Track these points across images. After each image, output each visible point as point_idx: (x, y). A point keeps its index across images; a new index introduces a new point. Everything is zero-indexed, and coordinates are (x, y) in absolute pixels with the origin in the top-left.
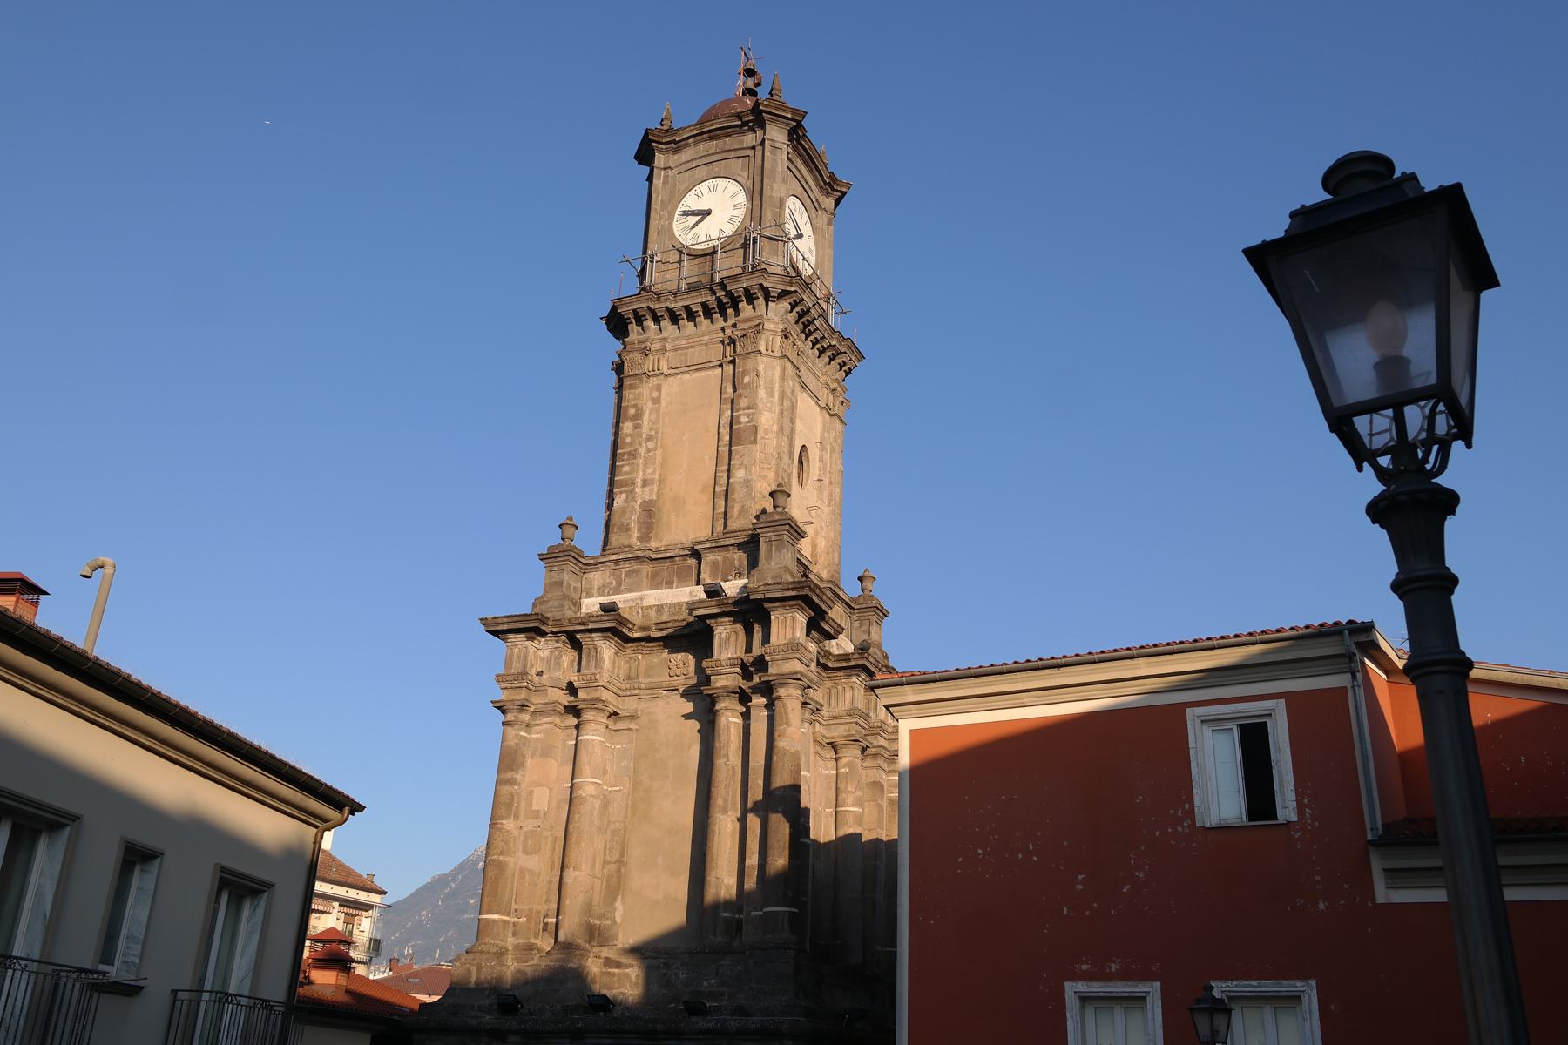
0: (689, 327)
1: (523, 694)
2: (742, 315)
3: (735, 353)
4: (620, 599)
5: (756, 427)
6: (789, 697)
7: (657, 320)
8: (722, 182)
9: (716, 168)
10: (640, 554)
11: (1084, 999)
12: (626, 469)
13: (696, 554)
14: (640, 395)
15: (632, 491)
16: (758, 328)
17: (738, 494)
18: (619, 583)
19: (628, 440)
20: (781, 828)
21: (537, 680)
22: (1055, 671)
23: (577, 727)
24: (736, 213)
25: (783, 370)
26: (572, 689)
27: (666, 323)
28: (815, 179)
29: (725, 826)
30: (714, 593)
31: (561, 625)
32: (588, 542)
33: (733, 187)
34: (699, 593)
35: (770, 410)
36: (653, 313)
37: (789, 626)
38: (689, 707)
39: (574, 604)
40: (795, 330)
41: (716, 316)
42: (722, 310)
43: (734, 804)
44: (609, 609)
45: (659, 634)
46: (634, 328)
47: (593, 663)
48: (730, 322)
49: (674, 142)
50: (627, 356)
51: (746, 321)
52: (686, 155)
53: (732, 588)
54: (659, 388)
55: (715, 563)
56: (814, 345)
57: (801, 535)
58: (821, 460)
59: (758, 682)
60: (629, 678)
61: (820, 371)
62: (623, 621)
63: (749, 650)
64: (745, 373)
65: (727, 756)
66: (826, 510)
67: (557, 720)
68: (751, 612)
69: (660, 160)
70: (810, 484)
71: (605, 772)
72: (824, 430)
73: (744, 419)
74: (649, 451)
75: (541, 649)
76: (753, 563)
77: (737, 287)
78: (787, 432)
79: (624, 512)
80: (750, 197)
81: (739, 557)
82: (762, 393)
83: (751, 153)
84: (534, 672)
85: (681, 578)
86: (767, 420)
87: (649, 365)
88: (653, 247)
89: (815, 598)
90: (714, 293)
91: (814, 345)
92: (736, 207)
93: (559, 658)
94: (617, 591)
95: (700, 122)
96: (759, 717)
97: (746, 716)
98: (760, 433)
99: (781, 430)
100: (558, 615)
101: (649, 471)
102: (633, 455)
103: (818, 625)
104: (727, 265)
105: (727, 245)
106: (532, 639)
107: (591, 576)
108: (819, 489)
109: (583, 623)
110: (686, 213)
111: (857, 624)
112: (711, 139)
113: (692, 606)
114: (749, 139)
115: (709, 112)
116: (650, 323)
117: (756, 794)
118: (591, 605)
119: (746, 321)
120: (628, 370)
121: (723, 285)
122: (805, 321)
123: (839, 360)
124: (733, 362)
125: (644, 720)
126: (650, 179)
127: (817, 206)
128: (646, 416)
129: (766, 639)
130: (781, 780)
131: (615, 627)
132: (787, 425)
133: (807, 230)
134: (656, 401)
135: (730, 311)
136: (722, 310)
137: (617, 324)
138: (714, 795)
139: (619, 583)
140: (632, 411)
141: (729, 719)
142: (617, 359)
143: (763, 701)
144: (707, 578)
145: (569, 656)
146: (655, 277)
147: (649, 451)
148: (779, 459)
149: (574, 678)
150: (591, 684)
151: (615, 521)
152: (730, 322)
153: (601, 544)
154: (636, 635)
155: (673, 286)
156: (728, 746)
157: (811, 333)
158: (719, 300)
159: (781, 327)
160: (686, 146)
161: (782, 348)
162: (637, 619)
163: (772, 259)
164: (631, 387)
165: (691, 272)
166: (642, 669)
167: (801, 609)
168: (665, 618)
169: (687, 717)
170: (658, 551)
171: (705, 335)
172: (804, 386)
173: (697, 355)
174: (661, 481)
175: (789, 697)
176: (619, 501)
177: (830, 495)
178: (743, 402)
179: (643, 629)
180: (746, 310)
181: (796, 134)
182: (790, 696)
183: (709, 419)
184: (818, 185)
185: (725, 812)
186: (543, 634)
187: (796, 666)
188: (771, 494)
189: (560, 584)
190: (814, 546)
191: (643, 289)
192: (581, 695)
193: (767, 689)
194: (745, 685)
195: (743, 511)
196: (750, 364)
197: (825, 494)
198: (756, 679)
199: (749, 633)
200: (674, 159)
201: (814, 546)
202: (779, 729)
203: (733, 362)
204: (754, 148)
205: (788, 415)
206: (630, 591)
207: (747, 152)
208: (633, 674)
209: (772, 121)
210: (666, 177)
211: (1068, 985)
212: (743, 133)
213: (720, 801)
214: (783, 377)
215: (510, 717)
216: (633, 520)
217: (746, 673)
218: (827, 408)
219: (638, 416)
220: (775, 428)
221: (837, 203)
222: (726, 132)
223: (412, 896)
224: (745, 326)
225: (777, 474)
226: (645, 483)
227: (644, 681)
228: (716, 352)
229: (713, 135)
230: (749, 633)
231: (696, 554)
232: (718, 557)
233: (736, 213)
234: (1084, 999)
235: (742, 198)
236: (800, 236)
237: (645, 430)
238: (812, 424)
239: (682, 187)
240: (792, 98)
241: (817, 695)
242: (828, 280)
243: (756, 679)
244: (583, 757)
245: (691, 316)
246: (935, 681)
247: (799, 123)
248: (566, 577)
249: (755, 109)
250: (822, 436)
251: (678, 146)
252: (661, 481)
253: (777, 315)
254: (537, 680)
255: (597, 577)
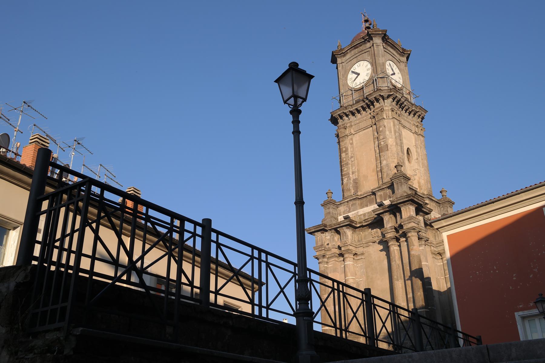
0: (358, 116)
1: (323, 252)
2: (376, 107)
3: (376, 121)
4: (350, 215)
5: (387, 145)
6: (412, 236)
7: (347, 116)
8: (362, 62)
9: (359, 58)
10: (355, 197)
11: (523, 318)
12: (345, 169)
13: (374, 193)
14: (346, 143)
15: (349, 177)
16: (382, 110)
17: (385, 170)
18: (350, 209)
19: (344, 159)
20: (418, 283)
21: (327, 246)
22: (492, 204)
23: (344, 260)
24: (368, 72)
25: (394, 122)
26: (340, 248)
27: (351, 116)
28: (397, 52)
29: (399, 285)
30: (381, 205)
31: (332, 226)
32: (337, 197)
33: (366, 63)
34: (376, 206)
35: (391, 138)
36: (345, 114)
37: (408, 211)
38: (381, 247)
39: (336, 219)
40: (396, 108)
41: (367, 109)
42: (369, 107)
43: (401, 277)
44: (346, 218)
45: (366, 224)
46: (340, 121)
47: (345, 237)
48: (372, 110)
49: (343, 53)
50: (339, 131)
51: (377, 109)
52: (348, 56)
53: (387, 202)
54: (352, 139)
55: (381, 196)
56: (406, 111)
57: (409, 179)
58: (417, 152)
59: (401, 234)
60: (359, 241)
61: (413, 120)
62: (352, 221)
63: (397, 223)
64: (380, 127)
65: (395, 261)
66: (422, 169)
67: (336, 259)
68: (394, 209)
69: (339, 60)
70: (413, 161)
71: (356, 274)
72: (416, 141)
73: (382, 143)
74: (352, 161)
75: (327, 237)
76: (393, 192)
77: (372, 98)
78: (399, 144)
79: (347, 184)
80: (372, 65)
81: (389, 191)
82: (387, 133)
83: (370, 50)
84: (326, 244)
85: (371, 203)
86: (391, 141)
87: (347, 132)
88: (342, 91)
89: (415, 200)
90: (364, 102)
91: (406, 111)
92: (368, 70)
93: (333, 238)
94: (349, 212)
95: (353, 42)
96: (404, 245)
97: (400, 246)
98: (389, 147)
99: (397, 144)
100: (330, 223)
101: (354, 168)
102: (347, 164)
103: (420, 209)
104: (367, 91)
105: (367, 85)
106: (323, 233)
107: (340, 208)
108: (418, 163)
109: (339, 224)
110: (353, 72)
111: (442, 209)
112: (355, 48)
113: (374, 211)
114: (368, 45)
115: (353, 39)
116: (345, 118)
117: (408, 274)
118: (341, 218)
119: (377, 109)
120: (340, 136)
121: (367, 98)
122: (400, 104)
123: (417, 114)
124: (375, 124)
125: (366, 254)
126: (337, 68)
127: (399, 61)
128: (349, 150)
129: (401, 218)
130: (415, 267)
131: (350, 224)
132: (399, 142)
133: (397, 71)
134: (352, 144)
135: (371, 107)
136: (369, 107)
137: (334, 121)
138: (393, 275)
139: (350, 209)
140: (344, 149)
141: (394, 248)
142: (336, 133)
143: (404, 239)
144: (378, 201)
145: (337, 237)
146: (344, 101)
147: (352, 161)
148: (398, 154)
149: (339, 244)
150: (345, 245)
151: (345, 188)
152: (372, 110)
153: (342, 197)
154: (358, 226)
155: (351, 103)
156: (395, 257)
157: (403, 107)
158: (367, 104)
159: (390, 108)
160: (347, 53)
161: (392, 115)
162: (357, 220)
163: (383, 85)
164: (343, 141)
165: (356, 96)
166: (363, 237)
167: (411, 204)
168: (367, 218)
169: (381, 251)
170: (361, 195)
171: (365, 115)
172: (404, 127)
173: (362, 125)
174: (358, 171)
175: (412, 236)
176: (345, 181)
177: (423, 163)
178: (381, 137)
179: (360, 223)
180: (377, 105)
181: (385, 38)
182: (413, 236)
183: (371, 147)
184: (398, 54)
185: (398, 280)
186: (326, 231)
187: (412, 225)
188: (395, 167)
189: (329, 213)
190: (419, 183)
191: (341, 107)
192: (343, 249)
193: (404, 235)
194: (397, 235)
195: (387, 175)
196: (381, 123)
197: (421, 164)
198: (401, 232)
199: (396, 216)
200: (344, 59)
201: (419, 183)
202: (411, 248)
203: (375, 124)
204: (370, 47)
205: (399, 137)
206: (354, 211)
207: (368, 50)
208: (360, 239)
209: (375, 36)
210: (342, 66)
211: (516, 313)
212: (366, 43)
213: (395, 277)
214: (394, 125)
215: (320, 260)
216: (351, 186)
217: (397, 231)
218: (416, 133)
219: (346, 151)
220: (394, 144)
221: (408, 58)
222: (360, 45)
223: (330, 361)
224: (377, 110)
225: (398, 160)
226: (353, 173)
227: (364, 241)
228: (369, 122)
229: (355, 47)
230: (396, 216)
231: (374, 193)
232: (381, 193)
233: (368, 72)
234: (523, 318)
235: (369, 66)
236: (394, 74)
237: (350, 155)
238: (410, 139)
239: (349, 68)
240: (381, 27)
241: (422, 234)
242: (409, 87)
243: (401, 232)
244: (347, 270)
245: (359, 112)
246: (451, 217)
247: (385, 35)
248: (331, 210)
249: (368, 34)
250: (415, 143)
251: (344, 54)
252: (358, 171)
253: (388, 104)
254: (327, 246)
255: (342, 208)
